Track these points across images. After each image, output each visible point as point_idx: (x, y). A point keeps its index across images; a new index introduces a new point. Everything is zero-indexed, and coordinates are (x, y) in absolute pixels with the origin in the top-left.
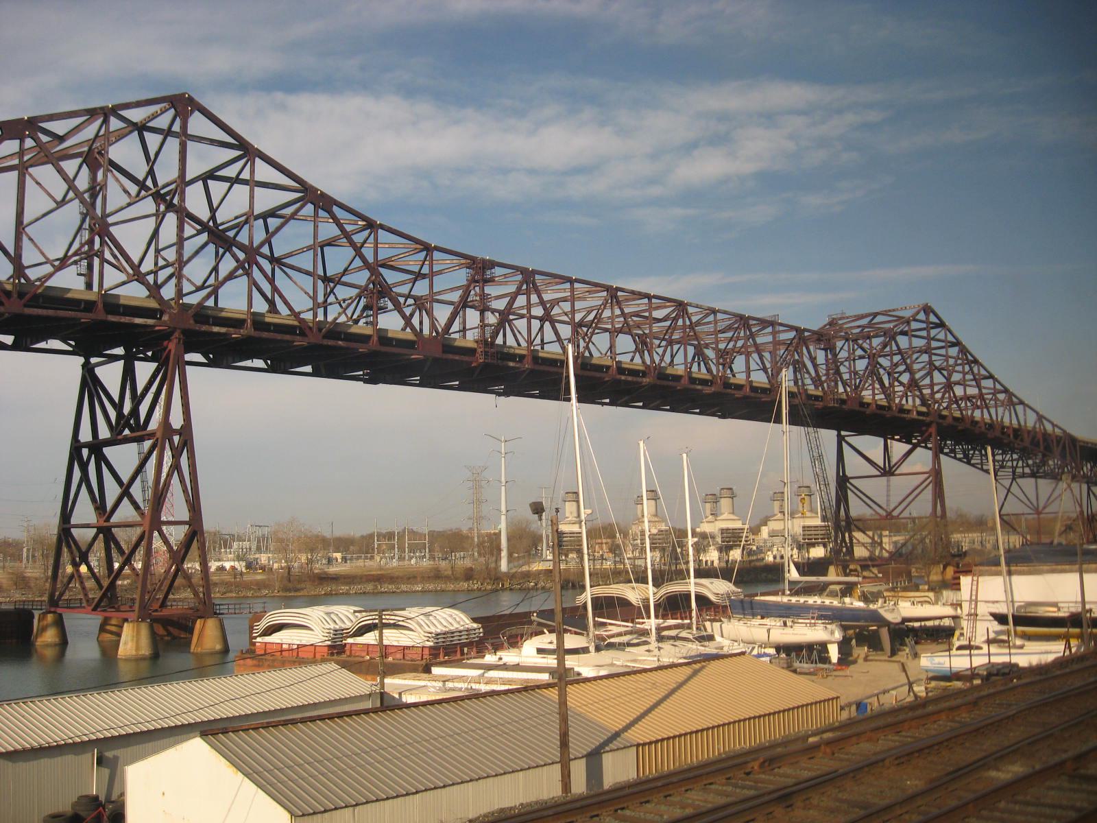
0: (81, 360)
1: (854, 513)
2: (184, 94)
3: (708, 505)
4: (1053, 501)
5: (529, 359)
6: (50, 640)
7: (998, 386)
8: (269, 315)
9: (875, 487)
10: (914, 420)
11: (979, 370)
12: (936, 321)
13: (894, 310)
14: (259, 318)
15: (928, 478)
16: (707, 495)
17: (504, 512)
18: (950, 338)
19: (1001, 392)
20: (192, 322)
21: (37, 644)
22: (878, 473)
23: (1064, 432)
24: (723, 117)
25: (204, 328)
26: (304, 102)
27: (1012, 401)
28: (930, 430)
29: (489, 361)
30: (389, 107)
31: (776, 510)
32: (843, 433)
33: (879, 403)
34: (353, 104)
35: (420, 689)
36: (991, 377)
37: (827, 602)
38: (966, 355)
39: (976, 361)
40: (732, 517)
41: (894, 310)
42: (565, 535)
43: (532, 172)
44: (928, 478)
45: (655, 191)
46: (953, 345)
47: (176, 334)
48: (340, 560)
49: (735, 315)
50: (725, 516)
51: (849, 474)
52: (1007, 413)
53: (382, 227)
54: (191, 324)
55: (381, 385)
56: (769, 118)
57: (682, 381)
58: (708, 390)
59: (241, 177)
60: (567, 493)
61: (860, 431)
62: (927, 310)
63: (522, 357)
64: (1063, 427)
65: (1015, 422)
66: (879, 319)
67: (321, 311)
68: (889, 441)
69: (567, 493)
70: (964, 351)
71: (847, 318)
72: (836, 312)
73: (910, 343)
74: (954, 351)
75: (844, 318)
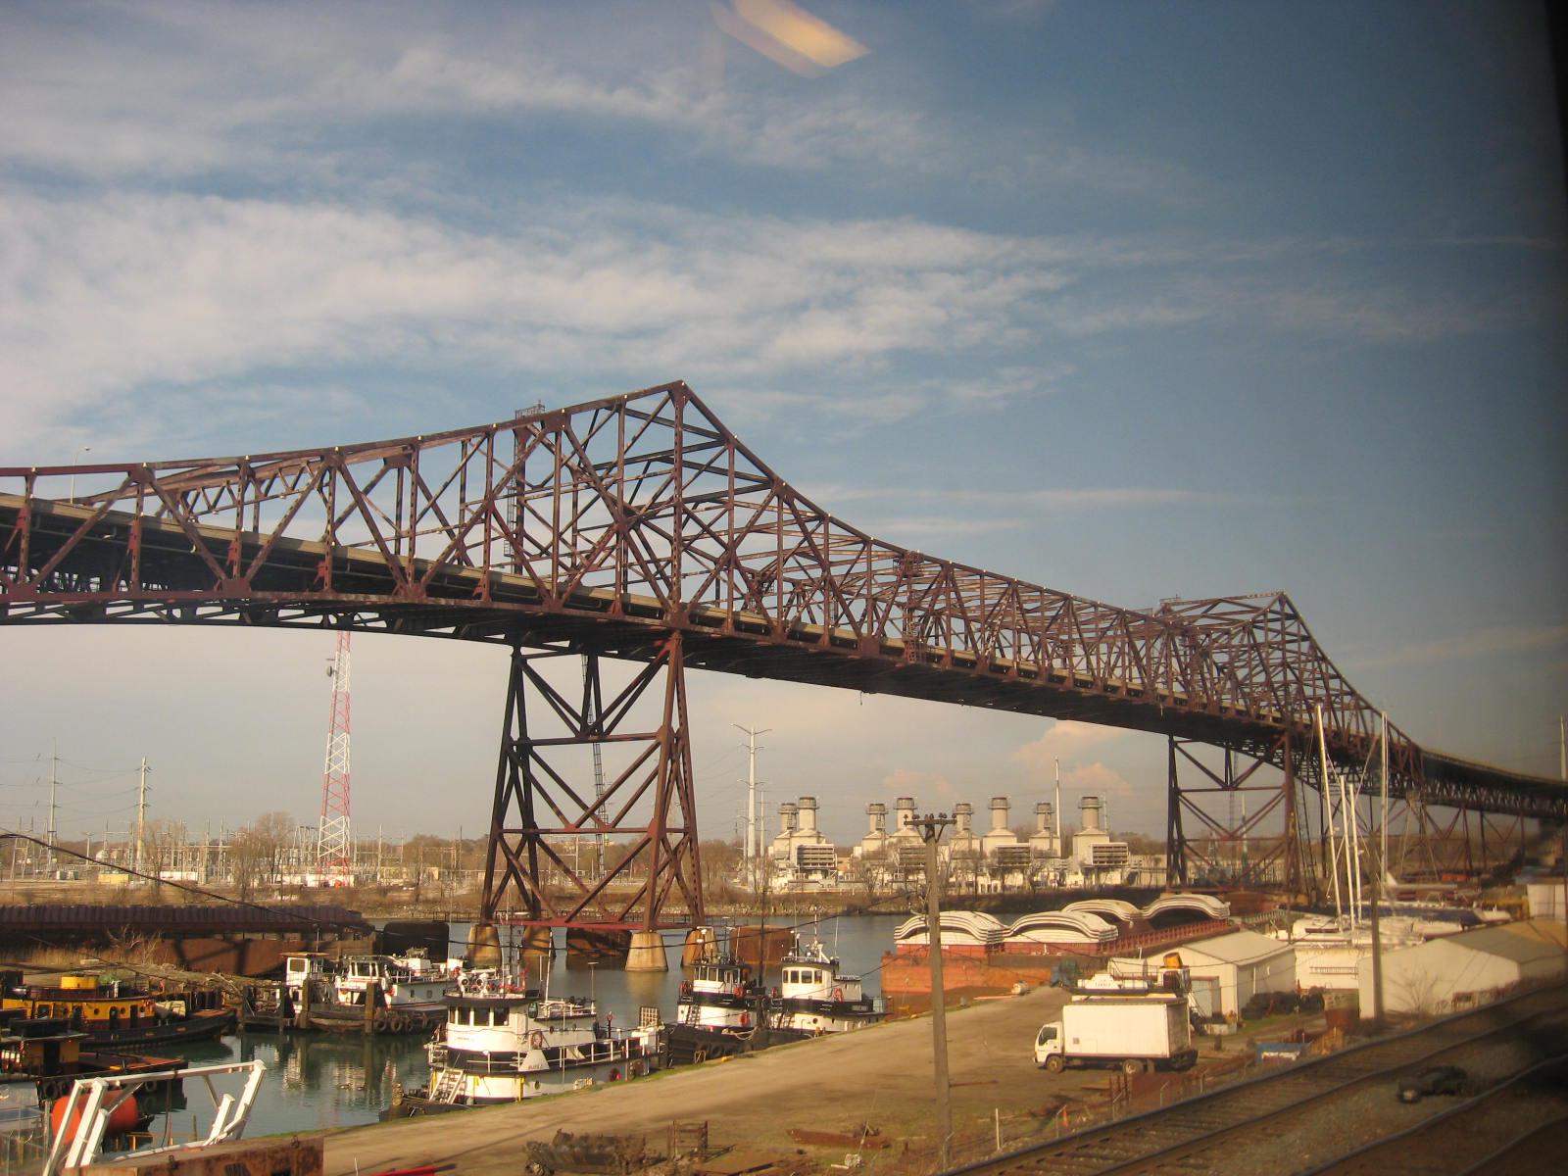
0: (510, 649)
1: (1187, 833)
2: (682, 382)
3: (873, 818)
5: (947, 660)
6: (490, 955)
7: (1345, 688)
8: (742, 613)
10: (1269, 727)
11: (1327, 669)
12: (1290, 612)
13: (1241, 598)
14: (152, 526)
16: (872, 805)
17: (753, 822)
19: (1347, 694)
20: (688, 622)
21: (476, 959)
22: (1220, 787)
23: (1408, 740)
24: (845, 270)
25: (698, 628)
26: (251, 213)
27: (1359, 705)
28: (667, 647)
29: (920, 662)
30: (375, 230)
31: (1041, 825)
32: (1176, 738)
34: (326, 221)
35: (53, 1124)
36: (1338, 676)
37: (1430, 905)
38: (1315, 651)
39: (1324, 659)
40: (1096, 832)
41: (1241, 598)
42: (805, 851)
43: (572, 331)
45: (747, 366)
47: (676, 635)
48: (436, 877)
49: (1111, 609)
50: (997, 832)
52: (1354, 719)
53: (832, 520)
54: (688, 625)
55: (878, 694)
56: (911, 275)
57: (1066, 683)
58: (763, 641)
59: (713, 465)
60: (801, 799)
61: (1195, 737)
62: (1283, 599)
63: (940, 657)
64: (1408, 736)
65: (1362, 730)
66: (1221, 608)
67: (405, 543)
68: (1232, 753)
69: (801, 799)
70: (1314, 647)
71: (1183, 603)
72: (1169, 595)
74: (1305, 646)
75: (1178, 604)
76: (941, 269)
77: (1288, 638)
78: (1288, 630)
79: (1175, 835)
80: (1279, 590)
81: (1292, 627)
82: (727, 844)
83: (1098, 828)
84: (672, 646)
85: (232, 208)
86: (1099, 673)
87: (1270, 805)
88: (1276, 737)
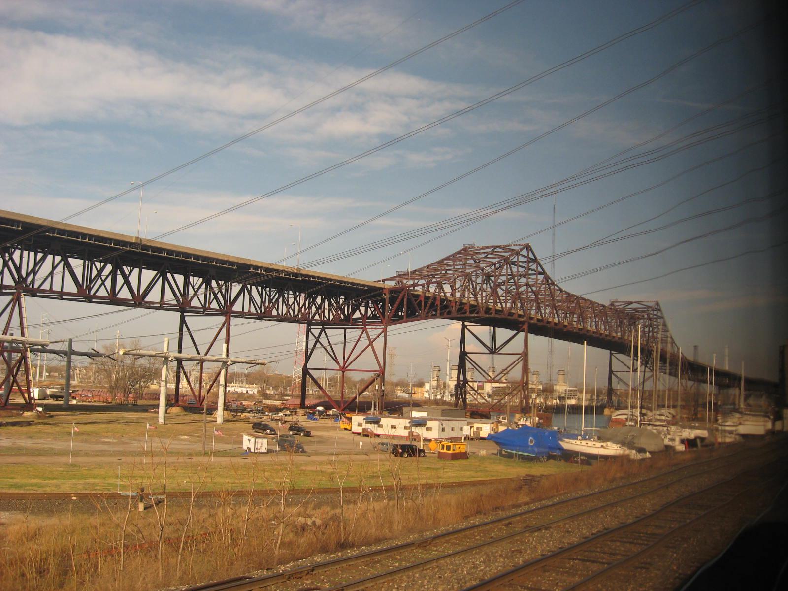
0: (462, 323)
4: (181, 334)
9: (484, 361)
15: (521, 357)
18: (540, 269)
26: (60, 42)
28: (524, 327)
30: (123, 55)
32: (613, 352)
33: (471, 303)
34: (96, 48)
40: (564, 384)
44: (521, 357)
46: (540, 274)
51: (467, 350)
56: (392, 98)
60: (453, 366)
62: (658, 304)
70: (547, 278)
71: (619, 302)
73: (518, 270)
74: (541, 277)
75: (472, 247)
76: (408, 96)
77: (530, 272)
78: (531, 268)
79: (462, 378)
80: (656, 300)
81: (534, 266)
82: (366, 379)
83: (564, 382)
84: (525, 327)
85: (50, 39)
86: (545, 316)
87: (513, 364)
88: (520, 325)
